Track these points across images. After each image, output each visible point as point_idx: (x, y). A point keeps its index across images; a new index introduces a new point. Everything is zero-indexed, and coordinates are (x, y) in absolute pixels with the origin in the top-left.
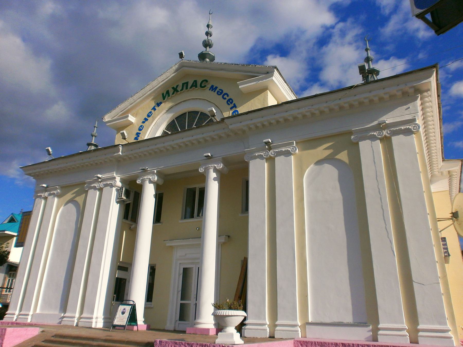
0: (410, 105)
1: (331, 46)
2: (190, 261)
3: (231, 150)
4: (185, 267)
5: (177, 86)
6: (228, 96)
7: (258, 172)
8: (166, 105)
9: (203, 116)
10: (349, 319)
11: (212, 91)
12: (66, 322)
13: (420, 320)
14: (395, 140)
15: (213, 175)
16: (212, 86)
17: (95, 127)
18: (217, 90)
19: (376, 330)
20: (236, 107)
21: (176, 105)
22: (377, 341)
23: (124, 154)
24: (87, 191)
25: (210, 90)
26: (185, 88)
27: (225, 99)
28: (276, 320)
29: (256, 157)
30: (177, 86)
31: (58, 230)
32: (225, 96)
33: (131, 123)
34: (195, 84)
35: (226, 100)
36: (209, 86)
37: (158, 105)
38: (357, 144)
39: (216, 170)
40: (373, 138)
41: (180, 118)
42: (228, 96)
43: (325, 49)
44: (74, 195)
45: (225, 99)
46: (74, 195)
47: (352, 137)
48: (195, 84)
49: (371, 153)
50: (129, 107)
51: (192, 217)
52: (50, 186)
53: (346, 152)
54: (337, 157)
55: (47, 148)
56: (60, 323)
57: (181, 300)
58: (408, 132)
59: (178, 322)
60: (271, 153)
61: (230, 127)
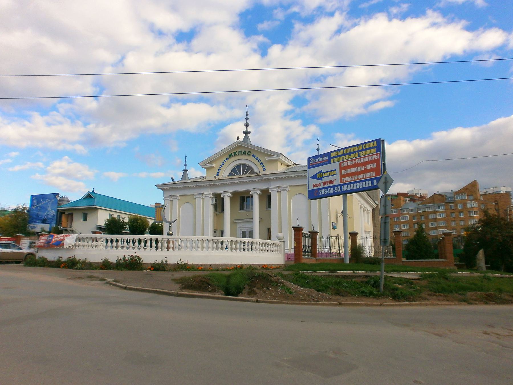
3: (264, 186)
34: (245, 153)
36: (252, 154)
37: (227, 159)
41: (238, 166)
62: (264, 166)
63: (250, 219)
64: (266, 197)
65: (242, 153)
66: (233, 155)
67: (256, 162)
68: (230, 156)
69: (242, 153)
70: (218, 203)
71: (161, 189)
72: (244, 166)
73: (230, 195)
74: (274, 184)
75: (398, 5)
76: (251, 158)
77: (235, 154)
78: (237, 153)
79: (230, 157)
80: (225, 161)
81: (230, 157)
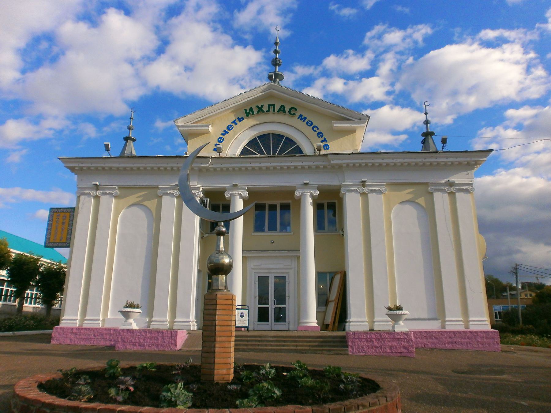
0: (469, 172)
1: (181, 18)
2: (267, 271)
3: (329, 181)
4: (286, 278)
5: (262, 106)
6: (318, 129)
7: (352, 204)
8: (248, 122)
9: (290, 142)
10: (426, 316)
11: (301, 120)
12: (154, 326)
13: (376, 315)
14: (459, 195)
15: (310, 200)
16: (301, 116)
17: (131, 119)
18: (307, 120)
19: (444, 322)
20: (326, 142)
21: (259, 124)
22: (468, 328)
23: (211, 166)
24: (161, 197)
25: (299, 118)
26: (271, 110)
27: (315, 131)
28: (85, 316)
29: (352, 191)
30: (262, 106)
31: (122, 235)
32: (315, 129)
33: (208, 132)
34: (282, 109)
35: (317, 133)
36: (298, 114)
37: (240, 120)
38: (432, 193)
39: (312, 196)
40: (444, 191)
41: (264, 137)
42: (318, 129)
43: (174, 20)
44: (141, 198)
45: (315, 131)
46: (141, 198)
47: (429, 188)
48: (271, 107)
49: (441, 200)
50: (207, 116)
51: (263, 230)
52: (103, 184)
53: (423, 198)
54: (417, 201)
55: (106, 143)
56: (149, 327)
57: (259, 304)
58: (467, 191)
59: (257, 323)
60: (366, 190)
61: (332, 162)
62: (325, 140)
63: (295, 251)
64: (330, 209)
65: (277, 109)
66: (255, 111)
67: (309, 130)
68: (249, 113)
69: (277, 109)
70: (216, 209)
71: (72, 169)
72: (278, 137)
73: (246, 194)
74: (350, 178)
75: (401, 23)
76: (295, 121)
77: (260, 110)
78: (265, 109)
79: (248, 115)
80: (234, 122)
81: (248, 115)
